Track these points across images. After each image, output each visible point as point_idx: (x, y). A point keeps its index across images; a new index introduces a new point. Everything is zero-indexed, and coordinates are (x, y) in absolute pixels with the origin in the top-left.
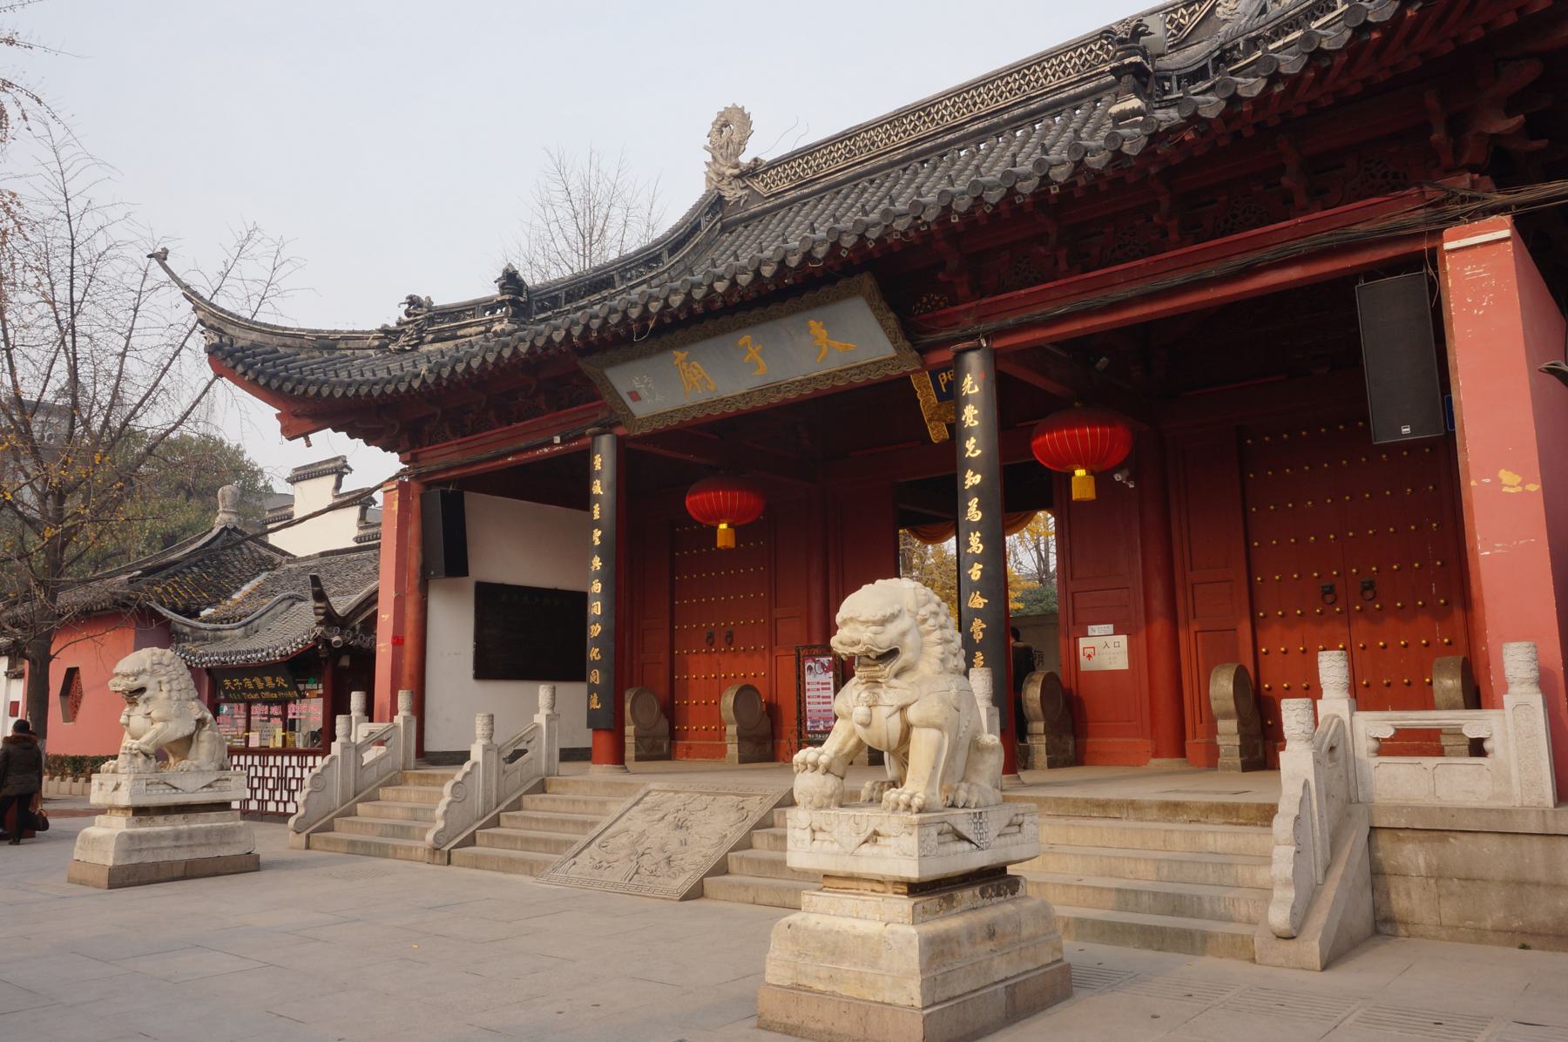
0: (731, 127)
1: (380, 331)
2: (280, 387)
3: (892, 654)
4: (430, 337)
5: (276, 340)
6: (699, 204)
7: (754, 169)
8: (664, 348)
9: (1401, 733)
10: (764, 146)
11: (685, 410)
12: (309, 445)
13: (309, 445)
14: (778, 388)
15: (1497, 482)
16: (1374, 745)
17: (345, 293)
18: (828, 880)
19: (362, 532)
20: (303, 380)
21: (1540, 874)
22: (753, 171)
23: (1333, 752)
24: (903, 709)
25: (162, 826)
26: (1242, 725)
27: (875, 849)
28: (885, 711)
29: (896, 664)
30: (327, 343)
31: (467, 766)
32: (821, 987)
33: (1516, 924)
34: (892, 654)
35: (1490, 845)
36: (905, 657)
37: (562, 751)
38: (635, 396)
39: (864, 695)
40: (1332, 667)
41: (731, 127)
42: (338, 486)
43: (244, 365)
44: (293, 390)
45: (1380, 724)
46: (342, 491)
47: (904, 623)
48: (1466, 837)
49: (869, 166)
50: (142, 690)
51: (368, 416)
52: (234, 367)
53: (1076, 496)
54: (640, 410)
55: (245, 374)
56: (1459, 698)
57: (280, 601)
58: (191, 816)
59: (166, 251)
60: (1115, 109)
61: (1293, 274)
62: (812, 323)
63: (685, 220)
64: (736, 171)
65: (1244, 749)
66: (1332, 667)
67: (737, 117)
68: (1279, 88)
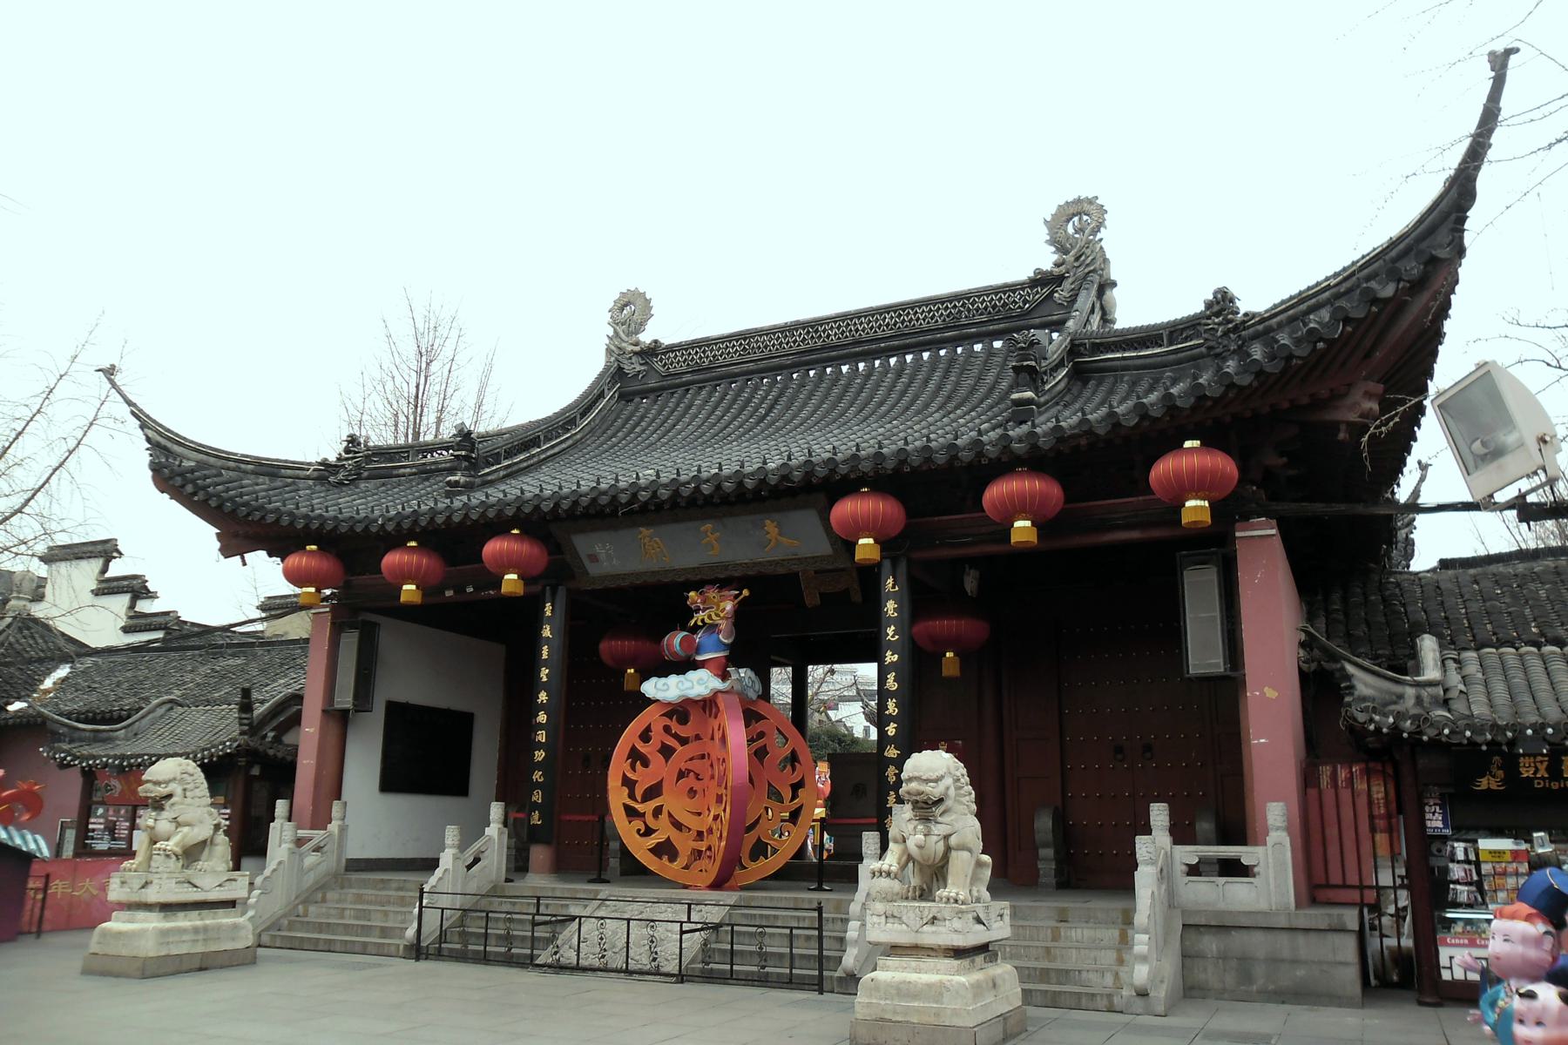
0: (631, 309)
1: (320, 464)
2: (234, 511)
3: (941, 801)
4: (366, 474)
5: (220, 463)
6: (601, 375)
7: (654, 349)
8: (635, 525)
9: (1203, 861)
10: (664, 329)
11: (638, 575)
12: (244, 564)
13: (244, 564)
14: (726, 567)
15: (1263, 694)
16: (1184, 868)
17: (293, 422)
18: (895, 950)
19: (131, 622)
20: (232, 499)
21: (1286, 954)
22: (652, 352)
23: (1165, 875)
24: (946, 837)
25: (184, 921)
26: (1056, 852)
27: (934, 928)
28: (935, 838)
29: (942, 808)
30: (270, 469)
31: (438, 872)
32: (899, 1018)
33: (1271, 987)
34: (941, 801)
35: (1258, 938)
36: (949, 803)
37: (349, 861)
38: (594, 558)
39: (920, 827)
40: (1159, 814)
41: (631, 309)
42: (105, 570)
43: (196, 485)
44: (248, 514)
45: (1189, 854)
46: (107, 575)
47: (948, 781)
48: (1244, 932)
49: (762, 364)
50: (169, 796)
51: (277, 537)
52: (183, 486)
53: (945, 673)
54: (594, 570)
55: (195, 494)
56: (1213, 836)
57: (164, 703)
58: (205, 912)
59: (113, 367)
60: (1015, 396)
61: (1135, 535)
62: (768, 522)
63: (591, 388)
64: (637, 349)
65: (1058, 872)
66: (1159, 814)
67: (639, 302)
68: (1146, 423)
